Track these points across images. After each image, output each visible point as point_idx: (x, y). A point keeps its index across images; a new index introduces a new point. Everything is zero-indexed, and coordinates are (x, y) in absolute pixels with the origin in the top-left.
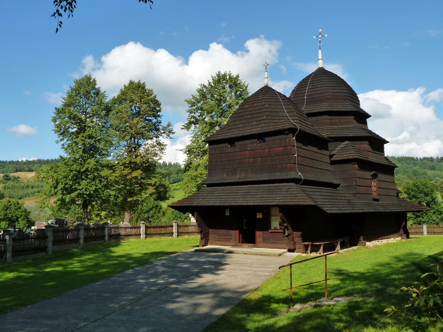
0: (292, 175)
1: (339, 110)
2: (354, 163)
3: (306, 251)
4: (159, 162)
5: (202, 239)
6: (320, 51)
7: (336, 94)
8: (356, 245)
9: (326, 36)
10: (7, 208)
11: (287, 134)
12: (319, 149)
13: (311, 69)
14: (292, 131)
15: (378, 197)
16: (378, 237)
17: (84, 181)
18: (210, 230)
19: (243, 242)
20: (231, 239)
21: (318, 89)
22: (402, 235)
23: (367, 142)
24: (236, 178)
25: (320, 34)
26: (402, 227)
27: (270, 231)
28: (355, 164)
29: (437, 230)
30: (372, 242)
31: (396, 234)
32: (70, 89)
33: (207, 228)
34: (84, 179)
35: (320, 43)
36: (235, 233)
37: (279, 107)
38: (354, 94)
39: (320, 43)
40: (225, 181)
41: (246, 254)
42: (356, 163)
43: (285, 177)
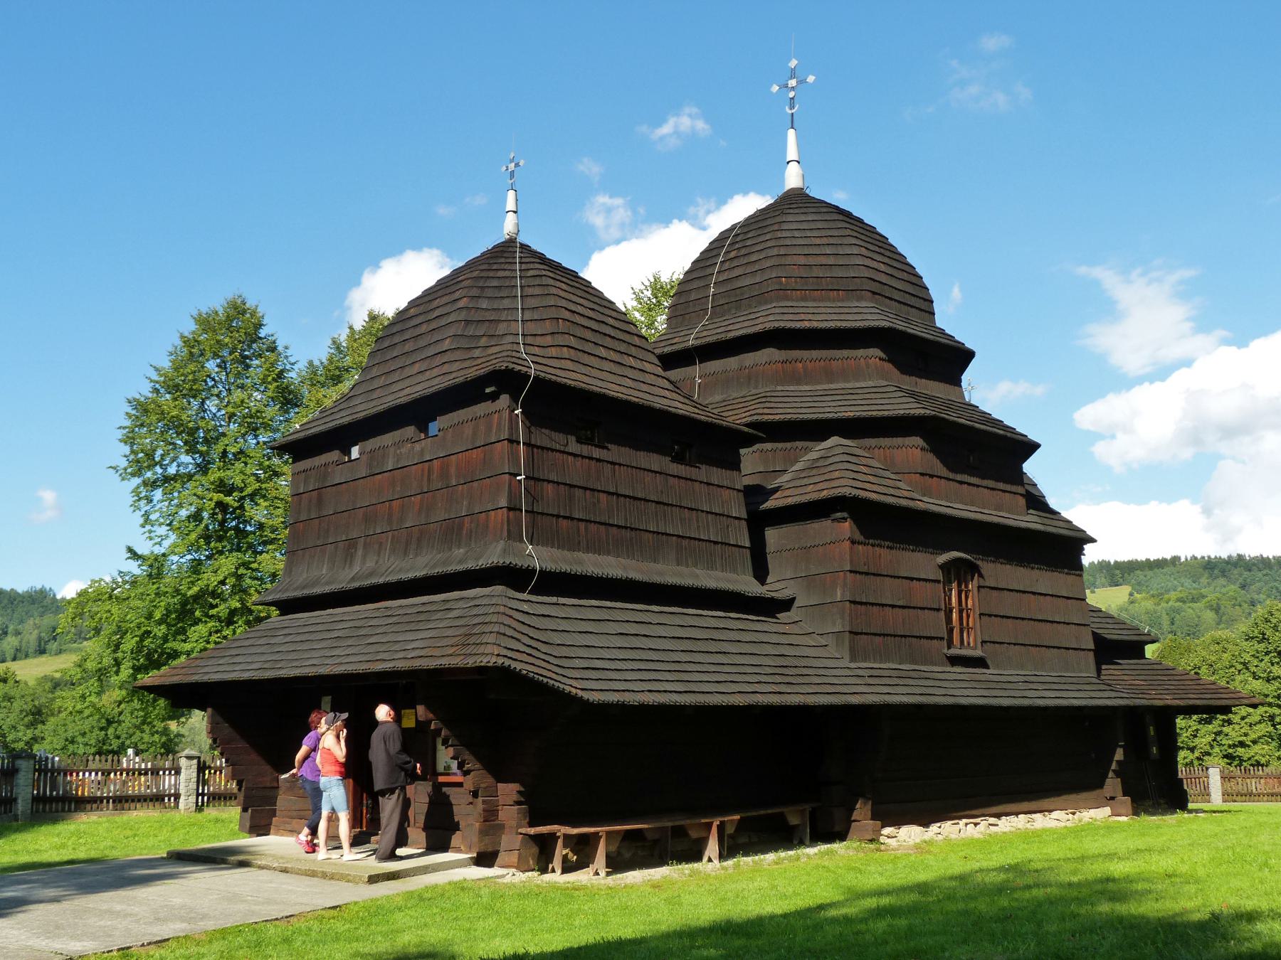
0: (493, 555)
1: (815, 325)
2: (839, 515)
4: (748, 544)
5: (245, 810)
8: (841, 836)
9: (811, 79)
10: (109, 722)
11: (494, 397)
12: (678, 459)
14: (506, 381)
15: (978, 653)
16: (976, 807)
17: (200, 627)
21: (754, 258)
22: (1112, 798)
23: (918, 441)
24: (344, 579)
25: (793, 74)
26: (1114, 766)
29: (1253, 785)
30: (934, 828)
32: (179, 343)
33: (268, 768)
34: (200, 620)
35: (792, 107)
37: (506, 303)
39: (792, 107)
40: (318, 590)
41: (285, 871)
42: (845, 515)
43: (470, 565)
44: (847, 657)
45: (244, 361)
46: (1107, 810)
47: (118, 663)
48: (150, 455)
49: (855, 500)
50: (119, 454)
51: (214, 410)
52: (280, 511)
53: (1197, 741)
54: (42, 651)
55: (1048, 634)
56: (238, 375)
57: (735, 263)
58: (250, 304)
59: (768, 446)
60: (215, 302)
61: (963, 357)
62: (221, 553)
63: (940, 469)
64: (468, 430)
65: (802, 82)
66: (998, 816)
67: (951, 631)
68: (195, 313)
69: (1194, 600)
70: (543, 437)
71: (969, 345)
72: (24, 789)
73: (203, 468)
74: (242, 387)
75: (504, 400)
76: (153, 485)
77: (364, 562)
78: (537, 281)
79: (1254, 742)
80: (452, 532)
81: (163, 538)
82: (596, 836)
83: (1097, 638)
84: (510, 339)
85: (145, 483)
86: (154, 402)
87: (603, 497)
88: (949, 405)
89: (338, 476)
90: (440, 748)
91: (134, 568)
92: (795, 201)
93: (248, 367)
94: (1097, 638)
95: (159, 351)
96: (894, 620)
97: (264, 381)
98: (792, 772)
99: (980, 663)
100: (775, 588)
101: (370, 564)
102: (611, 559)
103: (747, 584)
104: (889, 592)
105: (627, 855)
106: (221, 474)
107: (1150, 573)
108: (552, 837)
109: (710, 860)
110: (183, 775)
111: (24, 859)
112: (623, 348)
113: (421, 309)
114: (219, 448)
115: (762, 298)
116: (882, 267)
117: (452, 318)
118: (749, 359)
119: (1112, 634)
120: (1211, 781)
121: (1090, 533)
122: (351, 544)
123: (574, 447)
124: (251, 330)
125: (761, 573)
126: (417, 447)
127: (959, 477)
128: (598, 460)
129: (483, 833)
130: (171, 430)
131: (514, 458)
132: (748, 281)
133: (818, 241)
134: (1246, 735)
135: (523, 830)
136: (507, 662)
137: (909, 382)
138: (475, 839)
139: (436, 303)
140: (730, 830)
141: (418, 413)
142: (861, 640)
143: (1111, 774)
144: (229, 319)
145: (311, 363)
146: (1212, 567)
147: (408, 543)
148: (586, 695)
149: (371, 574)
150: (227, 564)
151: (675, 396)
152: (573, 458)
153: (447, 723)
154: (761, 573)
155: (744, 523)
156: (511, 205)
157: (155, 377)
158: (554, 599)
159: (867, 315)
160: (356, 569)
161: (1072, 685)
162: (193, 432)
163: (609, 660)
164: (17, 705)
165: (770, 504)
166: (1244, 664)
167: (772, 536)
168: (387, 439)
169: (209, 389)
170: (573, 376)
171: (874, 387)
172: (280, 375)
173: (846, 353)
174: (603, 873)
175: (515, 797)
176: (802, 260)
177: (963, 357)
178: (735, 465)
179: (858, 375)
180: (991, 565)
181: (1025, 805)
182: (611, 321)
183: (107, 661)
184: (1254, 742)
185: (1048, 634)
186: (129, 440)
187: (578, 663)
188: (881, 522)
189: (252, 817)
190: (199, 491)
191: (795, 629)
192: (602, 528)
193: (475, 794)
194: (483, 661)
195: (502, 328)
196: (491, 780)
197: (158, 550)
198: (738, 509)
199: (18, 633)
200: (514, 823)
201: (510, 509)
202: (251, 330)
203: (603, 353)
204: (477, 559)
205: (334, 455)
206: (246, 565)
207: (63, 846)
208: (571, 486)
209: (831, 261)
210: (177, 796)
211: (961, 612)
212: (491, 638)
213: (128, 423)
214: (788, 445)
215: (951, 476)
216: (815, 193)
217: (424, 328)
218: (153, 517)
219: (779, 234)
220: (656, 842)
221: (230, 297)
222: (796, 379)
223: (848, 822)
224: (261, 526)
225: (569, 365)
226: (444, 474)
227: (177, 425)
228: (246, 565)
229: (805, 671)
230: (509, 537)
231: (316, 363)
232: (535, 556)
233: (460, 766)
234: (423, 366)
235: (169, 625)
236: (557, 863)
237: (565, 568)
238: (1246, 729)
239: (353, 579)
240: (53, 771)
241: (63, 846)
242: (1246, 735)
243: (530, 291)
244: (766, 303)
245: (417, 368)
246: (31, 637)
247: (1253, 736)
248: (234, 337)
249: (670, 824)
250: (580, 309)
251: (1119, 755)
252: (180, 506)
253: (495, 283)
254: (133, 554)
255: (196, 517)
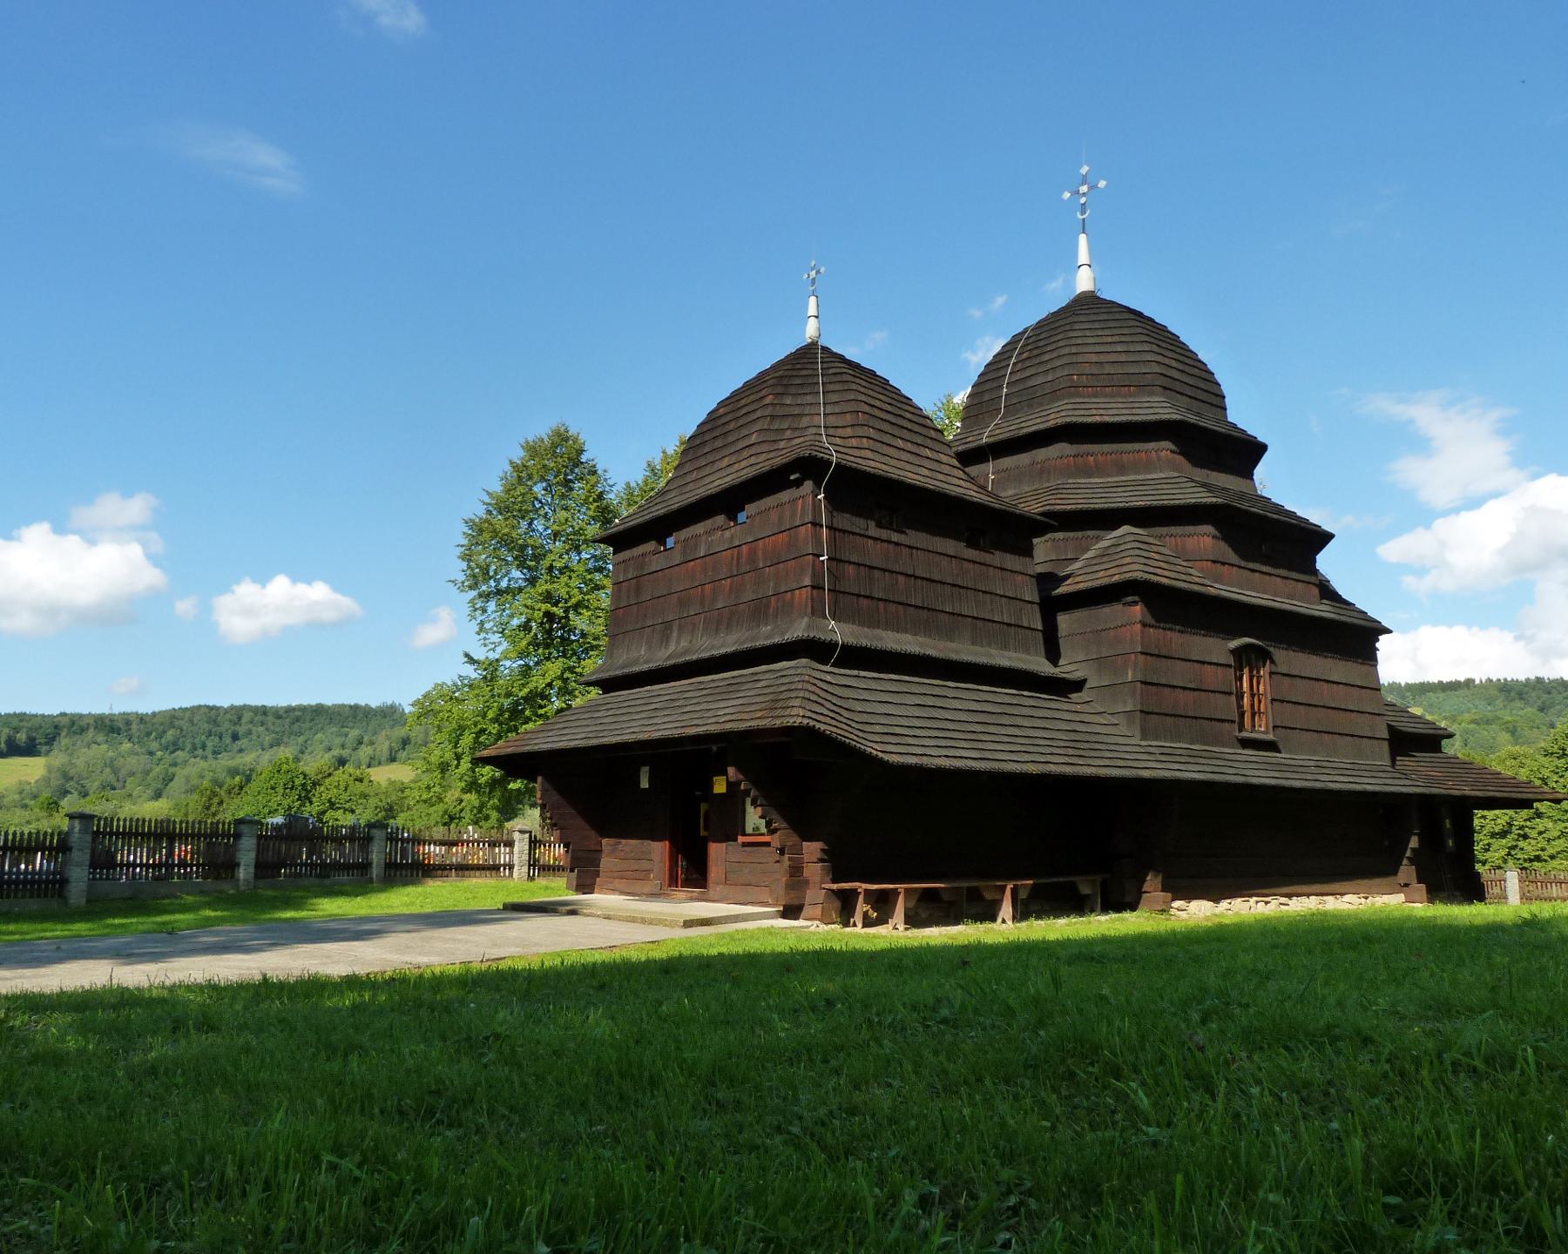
0: (798, 630)
1: (1107, 419)
2: (1130, 599)
3: (846, 917)
6: (1083, 238)
7: (1108, 369)
8: (1133, 907)
9: (1102, 184)
10: (452, 818)
11: (798, 484)
12: (972, 544)
13: (1054, 298)
14: (809, 467)
15: (1270, 737)
18: (604, 841)
19: (673, 882)
20: (649, 871)
21: (1046, 357)
22: (1406, 885)
23: (1209, 529)
25: (1084, 180)
26: (1408, 854)
27: (741, 839)
28: (1135, 603)
30: (1224, 904)
31: (1377, 881)
32: (509, 468)
33: (592, 833)
35: (1083, 213)
36: (659, 850)
37: (809, 399)
38: (1204, 375)
39: (1083, 213)
40: (636, 669)
41: (608, 918)
43: (777, 640)
44: (1138, 733)
45: (567, 483)
46: (1401, 897)
47: (458, 757)
48: (485, 571)
49: (1147, 583)
50: (457, 569)
51: (541, 528)
52: (601, 621)
53: (1488, 855)
54: (392, 759)
55: (1341, 722)
56: (563, 497)
57: (1028, 364)
58: (572, 431)
59: (1060, 535)
60: (540, 429)
61: (1253, 451)
62: (548, 659)
63: (1232, 557)
64: (774, 515)
65: (1093, 187)
66: (1290, 896)
67: (1242, 715)
68: (522, 441)
69: (1488, 722)
70: (845, 521)
71: (1261, 438)
72: (377, 855)
73: (532, 581)
74: (566, 509)
75: (808, 485)
76: (486, 596)
77: (678, 642)
78: (838, 378)
79: (1552, 857)
80: (760, 611)
81: (496, 645)
82: (895, 893)
83: (1391, 728)
84: (814, 430)
85: (480, 596)
86: (487, 521)
87: (901, 579)
88: (1242, 496)
89: (656, 563)
90: (750, 809)
91: (471, 672)
92: (1088, 304)
93: (571, 489)
94: (1391, 728)
95: (491, 479)
96: (1185, 701)
97: (586, 501)
98: (1087, 837)
99: (1271, 746)
100: (1068, 668)
101: (684, 643)
102: (909, 637)
103: (1043, 667)
104: (1179, 674)
105: (924, 916)
106: (548, 587)
107: (1442, 695)
108: (854, 894)
109: (1004, 921)
110: (516, 849)
111: (377, 912)
112: (919, 440)
113: (729, 408)
114: (546, 563)
115: (1055, 395)
116: (1174, 364)
117: (759, 414)
118: (1042, 454)
119: (1407, 727)
120: (1509, 884)
121: (1385, 624)
122: (668, 625)
123: (873, 531)
124: (574, 455)
125: (1053, 655)
126: (727, 534)
127: (1251, 565)
128: (897, 544)
129: (790, 887)
130: (503, 547)
131: (817, 540)
132: (1040, 380)
133: (1109, 339)
134: (1543, 850)
135: (827, 886)
136: (812, 723)
137: (1201, 474)
138: (781, 891)
139: (743, 402)
140: (1023, 895)
141: (729, 502)
142: (1152, 719)
143: (1405, 862)
144: (554, 446)
145: (628, 484)
146: (1510, 691)
147: (719, 623)
148: (886, 757)
149: (686, 652)
150: (554, 668)
151: (968, 485)
152: (874, 542)
153: (756, 783)
154: (1053, 655)
155: (1036, 608)
156: (812, 310)
157: (488, 500)
158: (855, 672)
159: (1157, 408)
160: (672, 648)
161: (1371, 773)
162: (523, 548)
163: (907, 727)
164: (373, 801)
165: (1062, 590)
166: (1542, 779)
167: (1064, 621)
168: (699, 528)
169: (537, 510)
170: (872, 464)
171: (1166, 478)
172: (600, 497)
173: (1137, 446)
174: (901, 927)
175: (819, 855)
176: (1094, 358)
177: (1253, 451)
178: (1028, 552)
179: (1148, 467)
180: (1284, 653)
181: (1305, 889)
182: (908, 416)
183: (449, 756)
184: (1552, 857)
185: (1341, 722)
186: (467, 557)
187: (878, 729)
188: (1172, 606)
189: (579, 877)
190: (529, 602)
191: (1086, 708)
192: (900, 608)
193: (782, 852)
194: (790, 721)
195: (805, 421)
196: (796, 839)
197: (493, 656)
198: (1031, 593)
199: (372, 743)
200: (818, 879)
201: (813, 587)
202: (574, 455)
203: (900, 443)
204: (783, 634)
205: (651, 546)
206: (571, 670)
207: (412, 904)
208: (871, 568)
209: (1123, 358)
210: (511, 867)
211: (1253, 696)
212: (797, 703)
213: (465, 542)
214: (1080, 534)
215: (1243, 564)
216: (1106, 295)
217: (732, 426)
218: (487, 626)
219: (1071, 334)
220: (951, 903)
221: (554, 426)
222: (1087, 472)
223: (1140, 893)
224: (583, 635)
225: (869, 454)
226: (752, 557)
227: (507, 542)
228: (571, 670)
229: (1097, 746)
230: (813, 614)
231: (633, 485)
232: (837, 631)
233: (768, 825)
234: (734, 459)
235: (500, 724)
236: (858, 918)
237: (865, 642)
238: (1543, 844)
239: (669, 657)
240: (403, 840)
241: (412, 904)
242: (1543, 850)
243: (831, 387)
244: (1058, 400)
245: (726, 462)
246: (383, 747)
247: (1551, 851)
248: (561, 462)
249: (965, 884)
250: (878, 403)
251: (1414, 842)
252: (512, 616)
253: (798, 381)
254: (471, 660)
255: (526, 627)
